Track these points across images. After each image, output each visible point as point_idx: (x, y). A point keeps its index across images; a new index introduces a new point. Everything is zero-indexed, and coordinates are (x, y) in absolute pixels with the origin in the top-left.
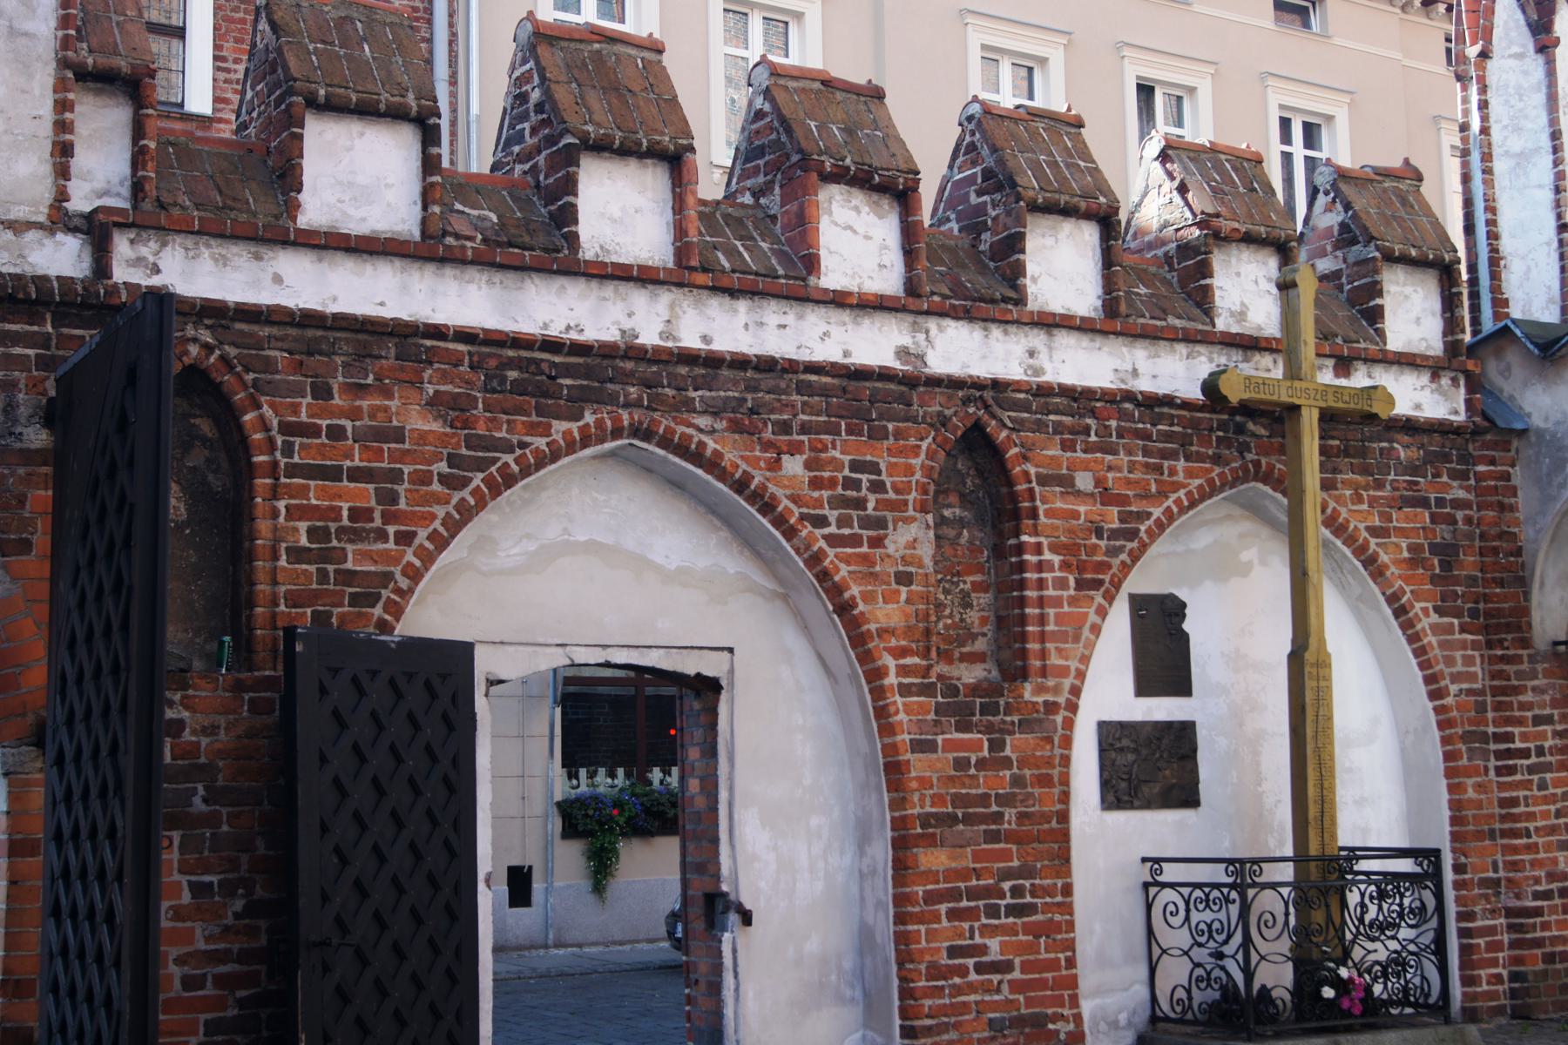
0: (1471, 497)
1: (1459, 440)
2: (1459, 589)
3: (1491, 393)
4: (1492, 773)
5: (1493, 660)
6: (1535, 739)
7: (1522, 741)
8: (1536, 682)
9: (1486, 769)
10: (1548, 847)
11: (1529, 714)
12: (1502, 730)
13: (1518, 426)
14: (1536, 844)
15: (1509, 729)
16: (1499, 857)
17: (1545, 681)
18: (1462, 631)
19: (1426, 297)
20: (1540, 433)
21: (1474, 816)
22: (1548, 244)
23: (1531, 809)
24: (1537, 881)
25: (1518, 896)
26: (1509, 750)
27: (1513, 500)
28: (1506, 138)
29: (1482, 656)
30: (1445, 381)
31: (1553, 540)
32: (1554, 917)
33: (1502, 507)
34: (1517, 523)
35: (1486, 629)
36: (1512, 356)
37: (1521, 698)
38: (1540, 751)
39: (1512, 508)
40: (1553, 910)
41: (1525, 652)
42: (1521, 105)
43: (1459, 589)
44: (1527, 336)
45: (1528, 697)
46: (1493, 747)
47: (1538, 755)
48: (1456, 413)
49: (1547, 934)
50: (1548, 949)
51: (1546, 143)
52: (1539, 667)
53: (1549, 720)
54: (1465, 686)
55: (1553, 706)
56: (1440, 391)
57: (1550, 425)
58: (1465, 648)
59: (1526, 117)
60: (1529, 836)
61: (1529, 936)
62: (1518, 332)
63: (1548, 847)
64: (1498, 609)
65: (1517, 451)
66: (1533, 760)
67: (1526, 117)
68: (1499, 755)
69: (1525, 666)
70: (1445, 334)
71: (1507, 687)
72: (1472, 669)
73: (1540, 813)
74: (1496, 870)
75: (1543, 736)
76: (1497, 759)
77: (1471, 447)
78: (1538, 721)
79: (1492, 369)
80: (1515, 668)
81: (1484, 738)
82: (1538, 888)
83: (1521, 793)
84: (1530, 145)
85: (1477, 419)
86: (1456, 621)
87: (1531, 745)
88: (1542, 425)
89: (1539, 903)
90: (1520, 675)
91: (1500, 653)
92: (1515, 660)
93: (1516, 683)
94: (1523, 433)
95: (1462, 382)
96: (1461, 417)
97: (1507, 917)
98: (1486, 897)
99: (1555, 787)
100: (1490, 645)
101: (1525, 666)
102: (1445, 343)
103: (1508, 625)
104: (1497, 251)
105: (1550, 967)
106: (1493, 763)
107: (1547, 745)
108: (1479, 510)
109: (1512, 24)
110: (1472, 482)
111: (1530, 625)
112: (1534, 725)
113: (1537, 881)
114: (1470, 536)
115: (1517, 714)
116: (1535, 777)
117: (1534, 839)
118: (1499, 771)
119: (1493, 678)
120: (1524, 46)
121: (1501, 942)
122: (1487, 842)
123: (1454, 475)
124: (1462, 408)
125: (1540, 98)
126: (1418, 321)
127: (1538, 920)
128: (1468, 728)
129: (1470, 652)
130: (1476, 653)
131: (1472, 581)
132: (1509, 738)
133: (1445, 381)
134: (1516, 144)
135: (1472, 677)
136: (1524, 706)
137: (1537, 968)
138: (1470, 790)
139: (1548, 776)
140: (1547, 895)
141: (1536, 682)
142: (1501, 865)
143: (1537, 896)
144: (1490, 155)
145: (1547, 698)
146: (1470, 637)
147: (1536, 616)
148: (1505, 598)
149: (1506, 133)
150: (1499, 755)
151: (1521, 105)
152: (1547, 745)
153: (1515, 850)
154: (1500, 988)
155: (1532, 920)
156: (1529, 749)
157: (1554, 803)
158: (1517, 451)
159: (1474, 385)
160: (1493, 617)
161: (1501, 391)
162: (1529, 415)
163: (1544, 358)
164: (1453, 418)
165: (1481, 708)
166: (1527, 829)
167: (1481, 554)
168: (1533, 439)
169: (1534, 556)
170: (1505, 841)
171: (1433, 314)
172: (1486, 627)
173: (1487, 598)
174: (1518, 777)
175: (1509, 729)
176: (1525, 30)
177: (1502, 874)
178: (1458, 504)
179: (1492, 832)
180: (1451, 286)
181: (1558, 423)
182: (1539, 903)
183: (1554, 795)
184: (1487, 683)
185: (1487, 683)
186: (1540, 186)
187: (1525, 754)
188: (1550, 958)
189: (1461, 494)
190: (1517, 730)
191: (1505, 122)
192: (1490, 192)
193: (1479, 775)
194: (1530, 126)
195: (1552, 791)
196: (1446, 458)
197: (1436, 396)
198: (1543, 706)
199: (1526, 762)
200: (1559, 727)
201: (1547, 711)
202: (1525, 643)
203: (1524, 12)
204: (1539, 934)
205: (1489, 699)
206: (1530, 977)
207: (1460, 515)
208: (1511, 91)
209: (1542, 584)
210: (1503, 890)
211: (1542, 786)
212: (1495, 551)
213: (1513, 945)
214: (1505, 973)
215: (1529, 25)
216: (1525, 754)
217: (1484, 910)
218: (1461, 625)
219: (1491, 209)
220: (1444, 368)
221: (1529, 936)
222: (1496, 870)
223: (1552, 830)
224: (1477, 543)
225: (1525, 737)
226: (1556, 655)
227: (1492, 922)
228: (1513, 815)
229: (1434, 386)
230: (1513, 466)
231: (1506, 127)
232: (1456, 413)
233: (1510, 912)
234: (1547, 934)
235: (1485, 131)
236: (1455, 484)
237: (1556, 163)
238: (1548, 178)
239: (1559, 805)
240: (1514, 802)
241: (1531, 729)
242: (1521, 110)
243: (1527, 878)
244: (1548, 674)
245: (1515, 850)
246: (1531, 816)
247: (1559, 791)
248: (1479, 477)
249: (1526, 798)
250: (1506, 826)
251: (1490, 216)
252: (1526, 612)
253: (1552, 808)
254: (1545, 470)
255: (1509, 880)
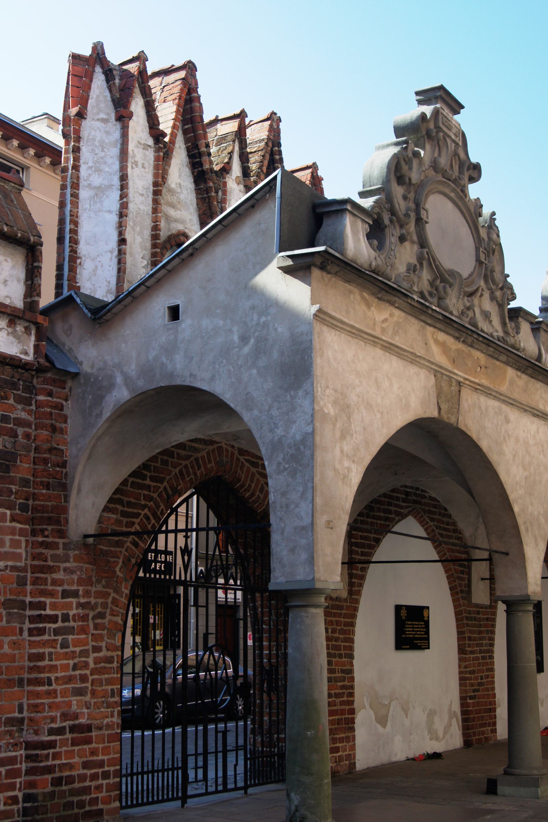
0: (31, 419)
1: (26, 374)
2: (14, 488)
3: (56, 346)
4: (26, 633)
5: (35, 545)
6: (62, 608)
7: (51, 609)
8: (67, 565)
9: (21, 630)
10: (64, 693)
11: (60, 589)
12: (37, 600)
13: (72, 370)
14: (55, 691)
15: (43, 599)
16: (25, 701)
17: (76, 564)
18: (13, 520)
19: (13, 267)
20: (87, 376)
21: (7, 668)
22: (111, 252)
23: (53, 663)
24: (53, 720)
25: (36, 733)
26: (40, 615)
27: (63, 425)
28: (90, 175)
29: (27, 541)
30: (20, 328)
31: (89, 458)
32: (64, 748)
33: (54, 429)
34: (65, 443)
35: (32, 521)
36: (74, 320)
37: (54, 576)
38: (66, 618)
39: (62, 431)
40: (64, 743)
41: (61, 541)
42: (102, 154)
43: (14, 488)
44: (84, 303)
45: (60, 576)
46: (28, 613)
47: (63, 621)
48: (26, 353)
49: (57, 762)
50: (57, 775)
51: (116, 181)
52: (72, 553)
53: (75, 594)
54: (10, 563)
55: (79, 583)
56: (14, 334)
57: (95, 371)
58: (13, 534)
59: (105, 163)
60: (50, 684)
61: (42, 764)
62: (78, 300)
63: (64, 693)
64: (43, 506)
65: (70, 390)
66: (60, 624)
67: (105, 163)
68: (33, 620)
69: (60, 552)
70: (25, 297)
71: (44, 566)
72: (18, 551)
73: (62, 666)
74: (21, 711)
75: (69, 606)
76: (31, 622)
77: (35, 381)
78: (66, 594)
79: (60, 329)
80: (52, 552)
81: (22, 605)
82: (53, 725)
83: (47, 650)
84: (106, 182)
85: (42, 361)
86: (8, 512)
87: (59, 613)
88: (89, 370)
89: (53, 738)
90: (55, 558)
91: (40, 539)
92: (54, 546)
93: (52, 564)
94: (75, 375)
95: (33, 332)
96: (30, 358)
97: (26, 749)
98: (10, 733)
99: (75, 646)
100: (34, 533)
101: (60, 552)
102: (24, 303)
103: (49, 518)
104: (76, 252)
105: (57, 789)
106: (27, 625)
107: (71, 613)
108: (36, 430)
109: (102, 98)
110: (33, 407)
111: (67, 521)
112: (63, 597)
113: (53, 720)
114: (27, 449)
115: (50, 588)
116: (60, 638)
117: (54, 686)
118: (31, 632)
119: (34, 559)
120: (108, 114)
121: (20, 769)
122: (16, 689)
123: (19, 400)
124: (31, 351)
125: (116, 151)
126: (5, 282)
127: (51, 751)
128: (9, 597)
129: (17, 537)
130: (23, 539)
131: (25, 482)
132: (41, 606)
133: (20, 328)
134: (96, 180)
135: (17, 557)
136: (55, 582)
137: (46, 790)
138: (6, 646)
139: (70, 637)
140: (60, 731)
141: (67, 565)
142: (25, 707)
143: (52, 732)
144: (78, 185)
145: (75, 577)
146: (19, 526)
147: (72, 514)
148: (49, 498)
149: (90, 172)
150: (33, 620)
151: (102, 154)
152: (71, 613)
153: (38, 695)
154: (15, 807)
155: (46, 752)
156: (57, 616)
157: (73, 658)
158: (70, 390)
159: (41, 335)
160: (38, 511)
161: (64, 345)
162: (81, 363)
163: (94, 319)
164: (22, 356)
165: (22, 582)
166: (49, 679)
167: (34, 463)
168: (82, 381)
169: (75, 468)
170: (31, 688)
171: (19, 281)
172: (33, 519)
173: (35, 497)
174: (46, 637)
175: (43, 599)
176: (110, 104)
177: (25, 714)
178: (19, 422)
179: (21, 681)
180: (34, 261)
181: (100, 369)
182: (53, 738)
183: (74, 652)
184: (29, 562)
185: (29, 562)
186: (110, 212)
187: (53, 619)
188: (57, 782)
189: (24, 415)
190: (48, 601)
191: (91, 164)
192: (75, 210)
193: (15, 635)
194: (107, 169)
195: (72, 649)
196: (14, 386)
197: (11, 338)
198: (71, 583)
199: (54, 626)
200: (82, 600)
201: (74, 587)
202: (62, 534)
203: (110, 91)
204: (50, 763)
205: (29, 575)
206: (40, 798)
207: (20, 431)
208: (97, 143)
209: (79, 491)
210: (25, 727)
211: (64, 645)
212: (45, 461)
213: (29, 772)
214: (20, 795)
215: (113, 100)
216: (53, 619)
217: (8, 744)
218: (11, 515)
219: (75, 223)
220: (20, 318)
221: (42, 764)
222: (21, 711)
223: (70, 679)
224: (32, 454)
225: (54, 606)
226: (86, 545)
227: (14, 754)
228: (38, 667)
229: (10, 330)
230: (66, 400)
231: (91, 168)
232: (26, 353)
233: (29, 745)
234: (57, 762)
235: (76, 167)
236: (19, 407)
237: (121, 197)
238: (116, 207)
239: (76, 661)
240: (40, 657)
241: (60, 600)
242: (102, 158)
243: (45, 718)
244: (77, 559)
245: (38, 695)
246: (53, 669)
247: (78, 649)
248: (39, 405)
249: (50, 654)
250: (33, 676)
251: (73, 227)
252: (65, 510)
253: (71, 662)
254: (88, 404)
255: (31, 719)
